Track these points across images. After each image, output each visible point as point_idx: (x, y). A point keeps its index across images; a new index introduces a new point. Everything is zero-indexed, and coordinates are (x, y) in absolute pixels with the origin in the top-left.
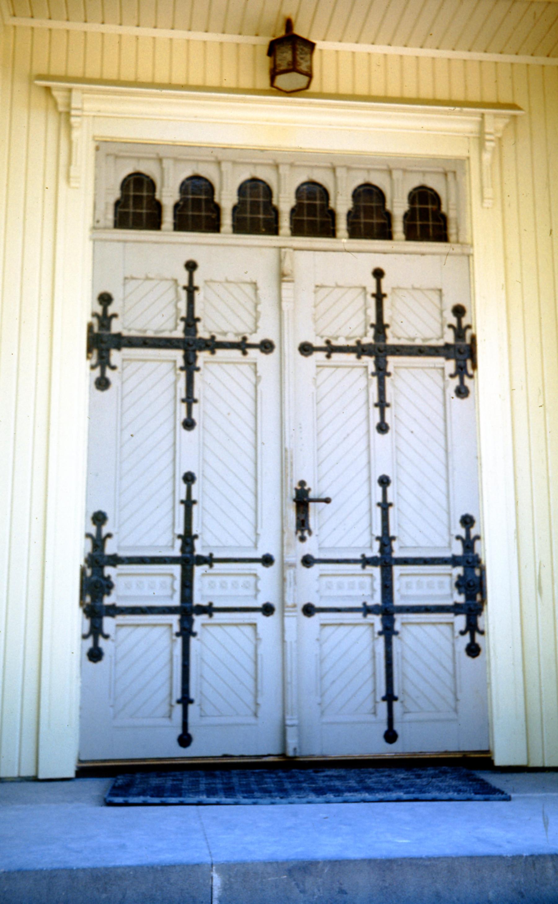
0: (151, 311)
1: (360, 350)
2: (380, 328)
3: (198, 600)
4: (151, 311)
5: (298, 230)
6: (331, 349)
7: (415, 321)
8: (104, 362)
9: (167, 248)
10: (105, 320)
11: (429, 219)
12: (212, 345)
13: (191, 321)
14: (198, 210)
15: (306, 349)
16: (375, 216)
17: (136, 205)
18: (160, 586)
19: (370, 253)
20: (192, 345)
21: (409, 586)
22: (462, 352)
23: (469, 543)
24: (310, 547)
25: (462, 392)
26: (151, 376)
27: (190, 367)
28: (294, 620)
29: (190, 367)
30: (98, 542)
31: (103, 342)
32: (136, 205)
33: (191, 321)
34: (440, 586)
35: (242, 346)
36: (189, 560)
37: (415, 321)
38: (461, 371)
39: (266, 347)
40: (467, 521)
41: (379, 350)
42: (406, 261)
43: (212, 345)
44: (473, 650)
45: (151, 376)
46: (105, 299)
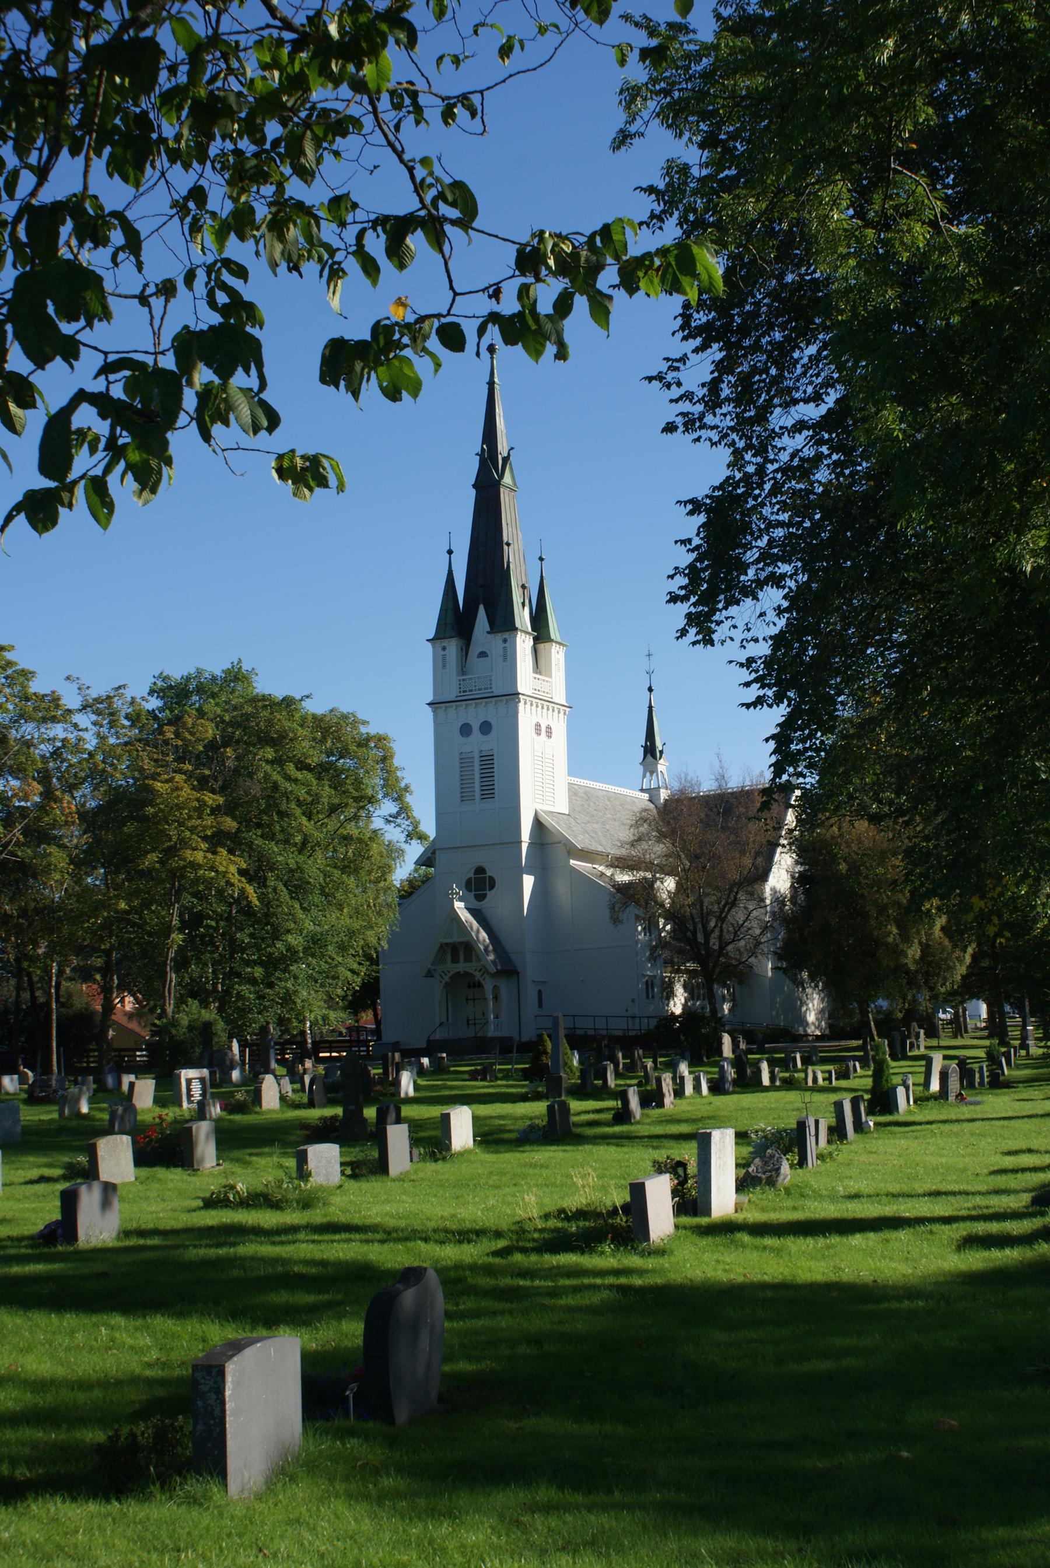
26: (471, 1002)
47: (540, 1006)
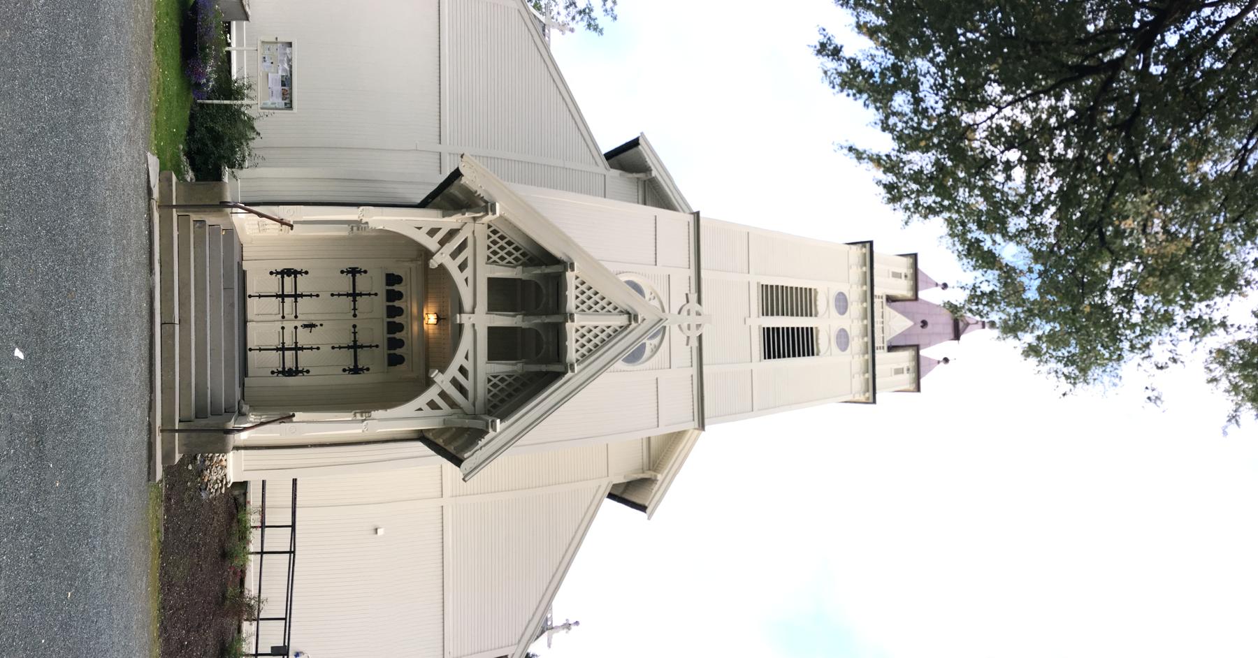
0: (363, 284)
1: (355, 341)
2: (362, 347)
3: (286, 299)
4: (363, 284)
5: (389, 323)
6: (355, 333)
7: (364, 358)
8: (348, 272)
9: (380, 287)
10: (360, 272)
11: (395, 360)
12: (354, 301)
13: (361, 295)
14: (393, 296)
15: (354, 326)
16: (501, 368)
17: (392, 279)
18: (289, 289)
19: (384, 344)
20: (354, 295)
21: (289, 289)
22: (356, 370)
23: (277, 273)
24: (300, 329)
25: (344, 370)
26: (345, 284)
27: (348, 295)
28: (279, 325)
29: (348, 295)
30: (300, 273)
31: (354, 272)
32: (392, 279)
33: (361, 295)
34: (288, 280)
35: (355, 309)
36: (296, 296)
37: (364, 358)
38: (350, 370)
39: (355, 316)
40: (271, 273)
41: (355, 347)
42: (382, 353)
43: (354, 301)
44: (306, 273)
45: (345, 284)
46: (365, 272)
47: (295, 481)
